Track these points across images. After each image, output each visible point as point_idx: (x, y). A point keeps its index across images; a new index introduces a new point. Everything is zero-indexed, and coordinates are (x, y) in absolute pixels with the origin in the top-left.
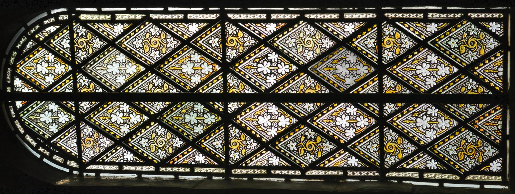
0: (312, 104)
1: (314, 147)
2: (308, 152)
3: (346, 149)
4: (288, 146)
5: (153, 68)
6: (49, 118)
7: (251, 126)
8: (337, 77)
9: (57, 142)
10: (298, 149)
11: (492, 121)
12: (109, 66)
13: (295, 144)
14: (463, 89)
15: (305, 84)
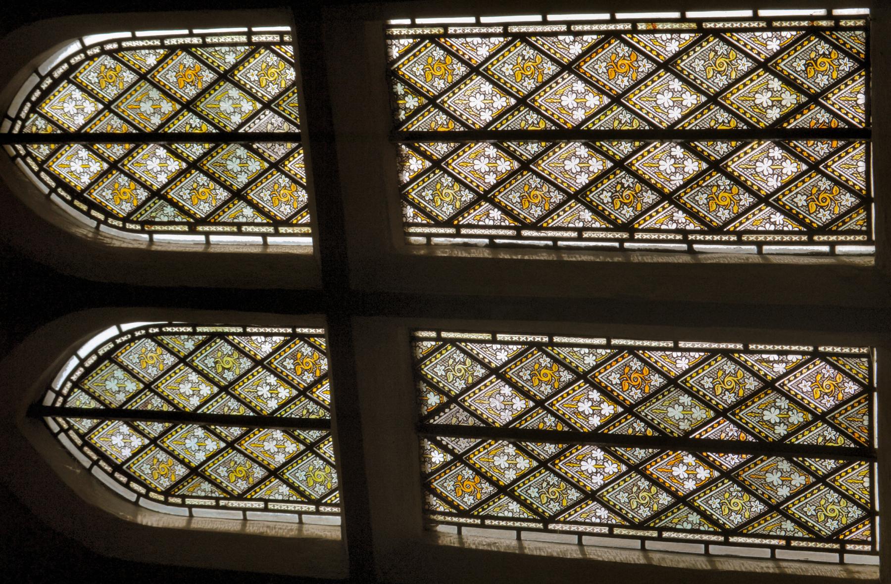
0: (725, 145)
1: (829, 200)
2: (625, 204)
3: (768, 204)
4: (795, 200)
5: (189, 106)
6: (78, 166)
7: (745, 175)
8: (140, 114)
9: (495, 196)
10: (613, 200)
11: (853, 165)
12: (472, 99)
13: (610, 194)
14: (523, 123)
15: (527, 121)
